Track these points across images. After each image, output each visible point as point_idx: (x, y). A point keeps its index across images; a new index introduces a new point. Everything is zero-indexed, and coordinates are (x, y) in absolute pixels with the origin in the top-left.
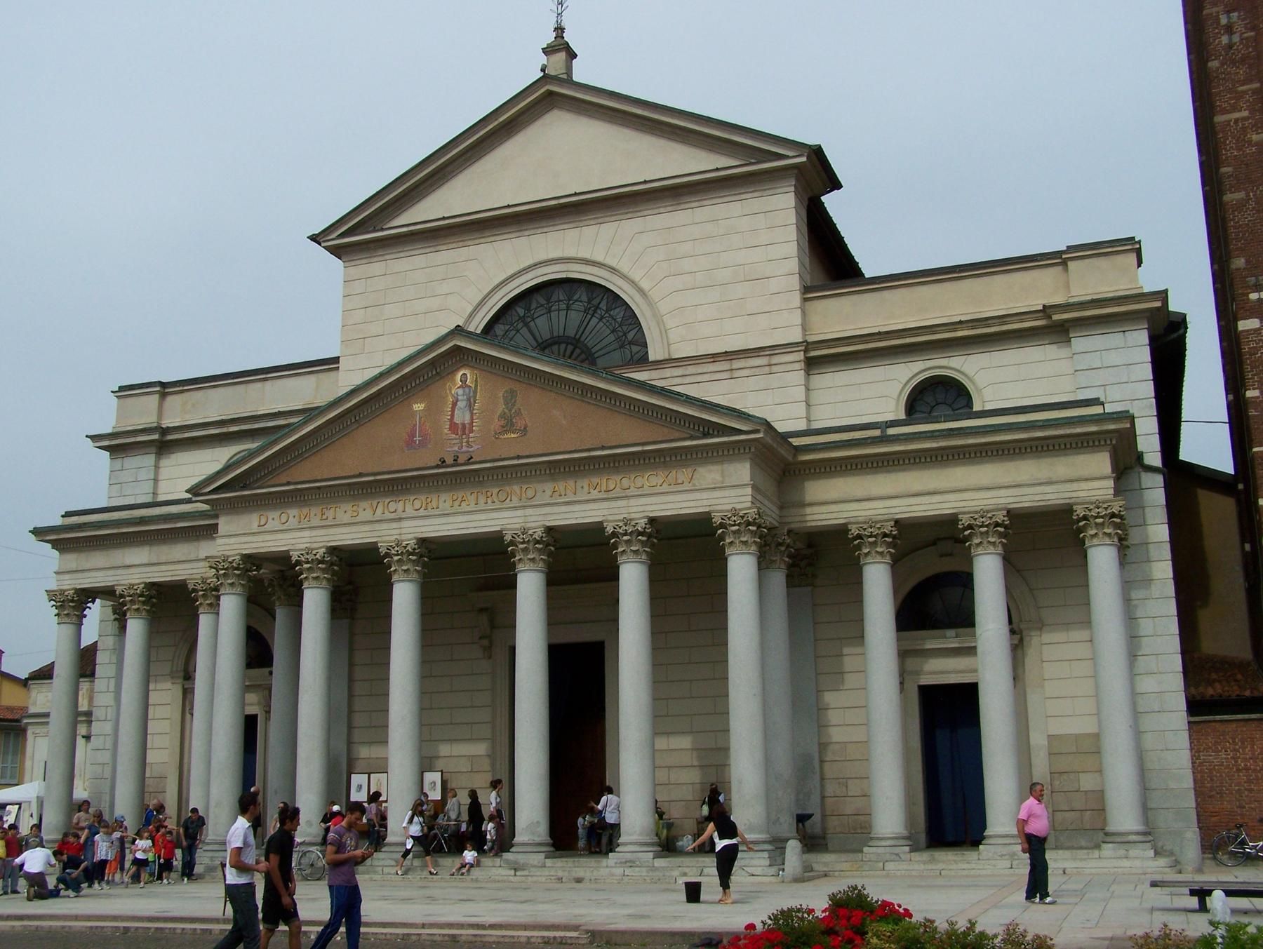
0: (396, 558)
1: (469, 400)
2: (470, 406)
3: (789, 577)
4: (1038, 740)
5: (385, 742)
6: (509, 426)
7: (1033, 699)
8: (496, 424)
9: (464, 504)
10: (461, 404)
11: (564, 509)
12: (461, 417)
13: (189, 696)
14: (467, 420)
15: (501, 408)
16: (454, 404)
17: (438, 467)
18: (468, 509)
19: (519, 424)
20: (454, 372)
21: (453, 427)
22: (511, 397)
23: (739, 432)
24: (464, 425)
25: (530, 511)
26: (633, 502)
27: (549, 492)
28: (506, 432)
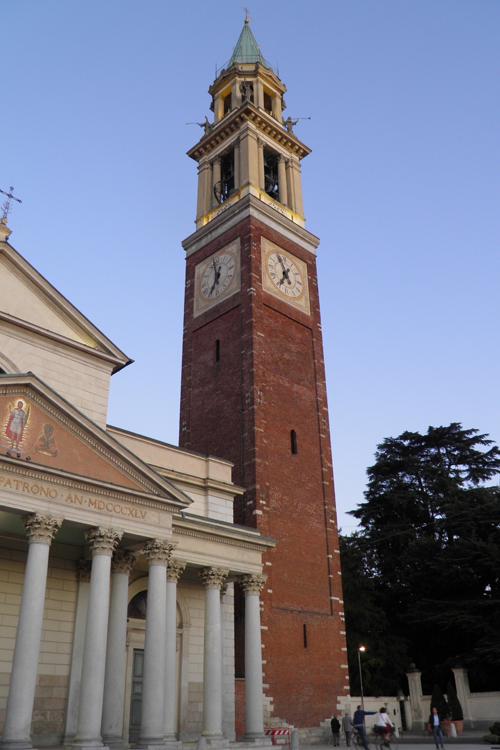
0: (50, 527)
1: (22, 419)
2: (23, 423)
3: (178, 586)
4: (185, 684)
5: (41, 678)
6: (46, 446)
7: (184, 662)
8: (38, 443)
9: (8, 486)
10: (16, 420)
11: (73, 511)
12: (15, 428)
13: (139, 659)
14: (19, 432)
15: (42, 434)
16: (12, 418)
17: (6, 456)
18: (10, 490)
19: (53, 449)
20: (14, 399)
21: (8, 432)
22: (49, 430)
23: (179, 501)
24: (16, 434)
25: (51, 505)
26: (113, 519)
27: (65, 497)
28: (43, 450)
